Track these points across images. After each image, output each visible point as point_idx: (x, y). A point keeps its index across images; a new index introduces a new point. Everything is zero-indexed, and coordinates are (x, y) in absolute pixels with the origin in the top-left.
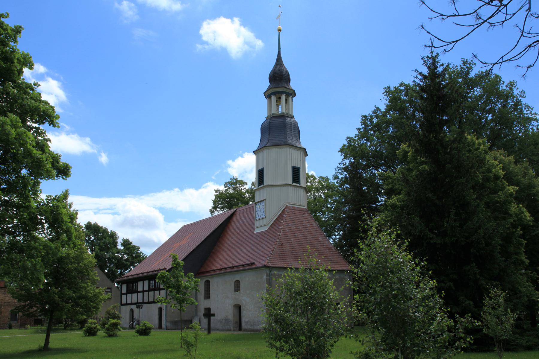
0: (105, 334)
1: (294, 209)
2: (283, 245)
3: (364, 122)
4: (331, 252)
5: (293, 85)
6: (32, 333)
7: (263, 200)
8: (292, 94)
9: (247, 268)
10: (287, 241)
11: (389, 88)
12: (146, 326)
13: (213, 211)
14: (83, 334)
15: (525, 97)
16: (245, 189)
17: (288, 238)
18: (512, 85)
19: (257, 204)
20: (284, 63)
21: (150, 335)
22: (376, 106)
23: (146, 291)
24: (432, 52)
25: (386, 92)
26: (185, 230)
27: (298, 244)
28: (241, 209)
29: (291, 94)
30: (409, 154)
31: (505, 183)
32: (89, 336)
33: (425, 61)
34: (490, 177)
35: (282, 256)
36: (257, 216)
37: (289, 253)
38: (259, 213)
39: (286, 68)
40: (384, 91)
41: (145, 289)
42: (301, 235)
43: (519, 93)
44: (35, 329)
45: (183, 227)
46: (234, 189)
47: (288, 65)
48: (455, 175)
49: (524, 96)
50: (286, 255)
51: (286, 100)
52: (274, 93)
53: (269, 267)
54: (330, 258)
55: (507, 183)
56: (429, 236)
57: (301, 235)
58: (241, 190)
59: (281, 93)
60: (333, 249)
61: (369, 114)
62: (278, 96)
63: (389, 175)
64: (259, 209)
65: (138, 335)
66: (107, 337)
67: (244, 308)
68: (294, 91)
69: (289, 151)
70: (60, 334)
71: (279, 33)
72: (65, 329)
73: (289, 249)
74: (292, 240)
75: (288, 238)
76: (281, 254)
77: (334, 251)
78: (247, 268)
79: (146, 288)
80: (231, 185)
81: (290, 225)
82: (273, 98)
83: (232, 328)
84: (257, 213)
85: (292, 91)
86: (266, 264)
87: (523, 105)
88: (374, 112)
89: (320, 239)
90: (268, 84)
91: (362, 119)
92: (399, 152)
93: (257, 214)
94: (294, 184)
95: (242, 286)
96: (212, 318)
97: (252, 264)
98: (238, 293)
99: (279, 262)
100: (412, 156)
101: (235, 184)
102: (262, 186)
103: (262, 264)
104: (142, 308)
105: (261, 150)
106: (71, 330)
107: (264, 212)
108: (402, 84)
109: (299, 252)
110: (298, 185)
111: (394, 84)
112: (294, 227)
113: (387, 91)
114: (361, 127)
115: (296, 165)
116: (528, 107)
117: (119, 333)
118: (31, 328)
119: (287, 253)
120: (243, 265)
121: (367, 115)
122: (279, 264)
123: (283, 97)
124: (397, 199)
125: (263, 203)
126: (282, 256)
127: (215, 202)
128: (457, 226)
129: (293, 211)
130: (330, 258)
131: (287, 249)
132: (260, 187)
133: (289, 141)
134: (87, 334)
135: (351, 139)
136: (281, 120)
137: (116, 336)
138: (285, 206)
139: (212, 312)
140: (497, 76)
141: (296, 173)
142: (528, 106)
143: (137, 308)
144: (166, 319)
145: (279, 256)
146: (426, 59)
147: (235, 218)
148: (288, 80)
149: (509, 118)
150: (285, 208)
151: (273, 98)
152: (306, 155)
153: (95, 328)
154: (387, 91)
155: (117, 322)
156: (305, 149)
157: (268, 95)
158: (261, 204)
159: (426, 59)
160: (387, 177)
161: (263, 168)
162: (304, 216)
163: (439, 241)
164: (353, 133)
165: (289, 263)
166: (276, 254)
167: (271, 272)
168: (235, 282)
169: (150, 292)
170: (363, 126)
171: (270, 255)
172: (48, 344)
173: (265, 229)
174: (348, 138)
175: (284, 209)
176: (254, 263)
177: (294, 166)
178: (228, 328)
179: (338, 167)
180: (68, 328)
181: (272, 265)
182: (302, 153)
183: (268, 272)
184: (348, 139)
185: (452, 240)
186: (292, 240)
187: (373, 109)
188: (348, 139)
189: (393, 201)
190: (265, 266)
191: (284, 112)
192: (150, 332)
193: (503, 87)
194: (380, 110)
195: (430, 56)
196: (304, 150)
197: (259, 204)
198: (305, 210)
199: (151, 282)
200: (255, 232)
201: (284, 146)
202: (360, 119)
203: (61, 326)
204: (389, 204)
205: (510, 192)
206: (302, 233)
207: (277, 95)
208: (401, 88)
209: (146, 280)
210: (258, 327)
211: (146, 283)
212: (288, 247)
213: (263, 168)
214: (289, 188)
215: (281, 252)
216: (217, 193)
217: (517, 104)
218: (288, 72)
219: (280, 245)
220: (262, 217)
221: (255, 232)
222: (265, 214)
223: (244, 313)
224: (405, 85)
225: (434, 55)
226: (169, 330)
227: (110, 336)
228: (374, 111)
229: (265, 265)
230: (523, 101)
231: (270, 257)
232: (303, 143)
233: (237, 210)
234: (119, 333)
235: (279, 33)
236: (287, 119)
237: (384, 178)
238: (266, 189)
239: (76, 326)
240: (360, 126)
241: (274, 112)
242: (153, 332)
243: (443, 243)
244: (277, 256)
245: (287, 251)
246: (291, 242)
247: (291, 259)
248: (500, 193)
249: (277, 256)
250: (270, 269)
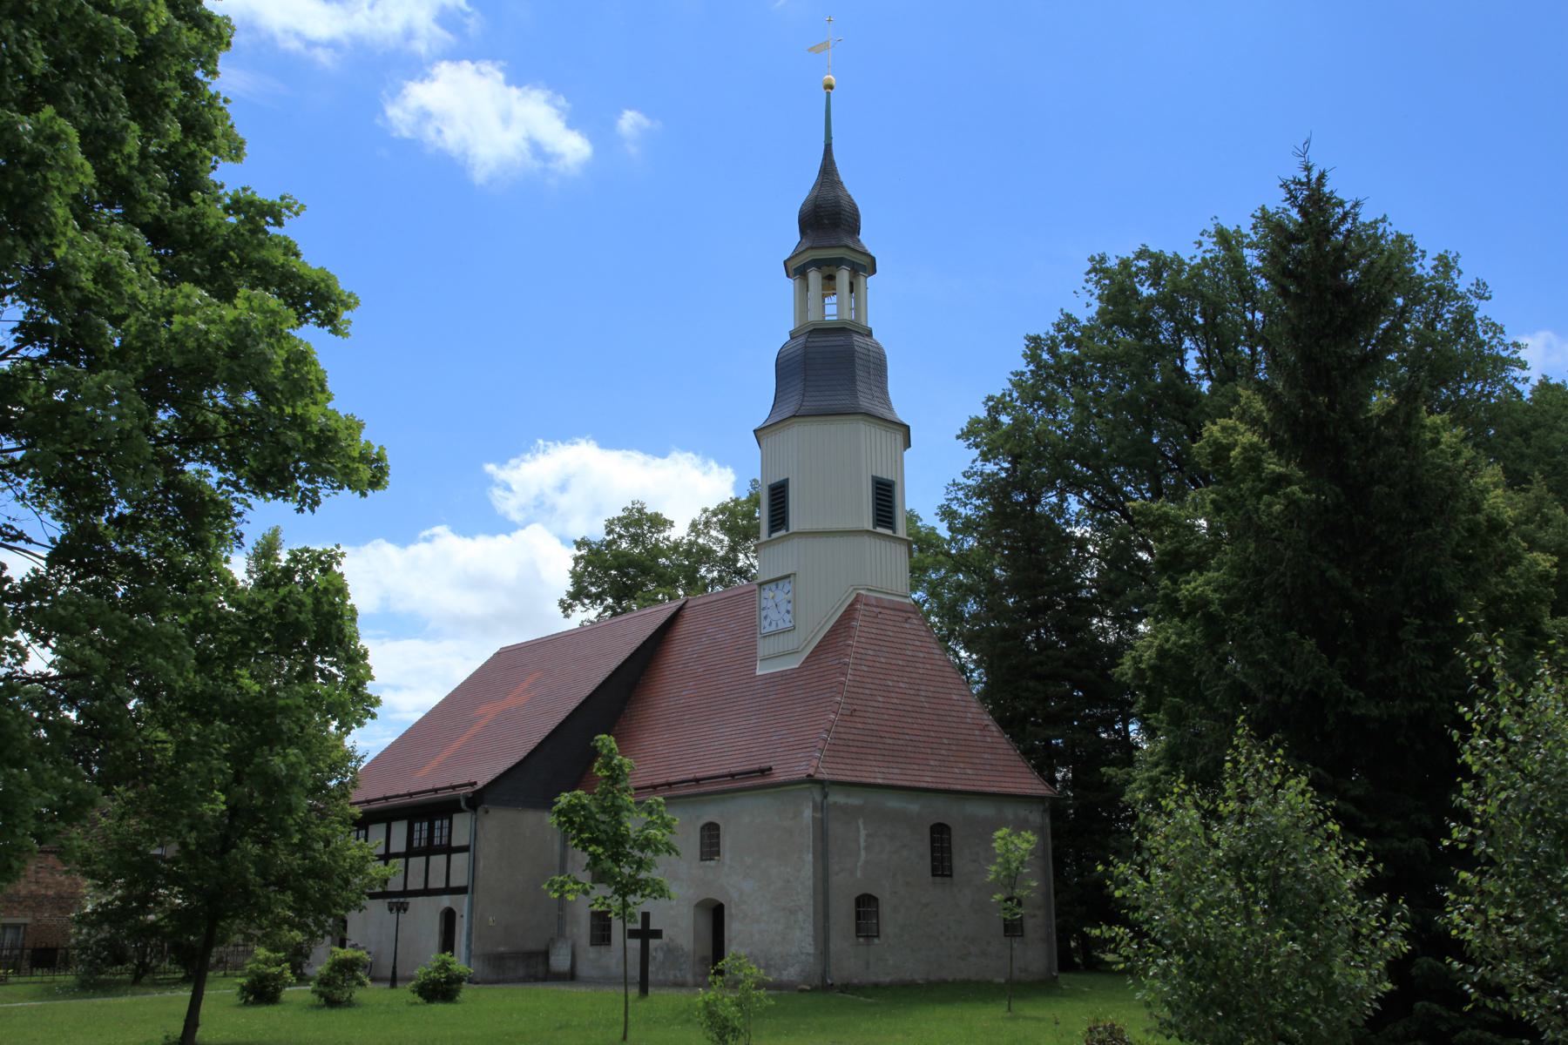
0: (315, 997)
1: (879, 604)
2: (857, 713)
3: (1033, 357)
4: (989, 739)
5: (869, 238)
6: (33, 998)
7: (788, 576)
8: (865, 266)
9: (748, 783)
10: (864, 703)
11: (1103, 259)
12: (447, 970)
13: (570, 606)
14: (238, 998)
15: (1490, 297)
16: (668, 539)
17: (867, 692)
18: (1445, 265)
19: (766, 587)
20: (843, 178)
21: (456, 1002)
22: (1065, 311)
23: (397, 855)
24: (1308, 169)
25: (1094, 270)
26: (507, 665)
27: (898, 713)
28: (701, 601)
29: (864, 268)
30: (1233, 453)
31: (1518, 544)
32: (253, 1004)
33: (1290, 192)
34: (1480, 523)
35: (854, 750)
36: (765, 623)
37: (874, 739)
38: (773, 614)
39: (849, 192)
40: (1088, 266)
41: (393, 850)
42: (901, 685)
43: (1473, 288)
44: (42, 982)
45: (498, 654)
46: (635, 540)
47: (855, 184)
48: (1404, 516)
49: (1487, 295)
50: (864, 744)
51: (851, 284)
52: (818, 264)
53: (821, 782)
54: (986, 756)
55: (1525, 544)
56: (1345, 694)
57: (901, 685)
58: (656, 545)
59: (838, 262)
60: (994, 729)
61: (1047, 333)
62: (827, 270)
63: (1165, 512)
64: (771, 603)
65: (419, 1000)
66: (319, 1007)
67: (733, 911)
68: (873, 260)
69: (866, 433)
70: (124, 1000)
71: (828, 94)
72: (137, 980)
73: (874, 727)
74: (880, 699)
75: (867, 692)
76: (851, 743)
77: (996, 734)
78: (748, 783)
79: (398, 844)
80: (626, 526)
81: (871, 652)
82: (814, 277)
83: (690, 978)
84: (764, 613)
85: (868, 260)
86: (811, 771)
87: (1479, 323)
88: (1059, 328)
89: (955, 697)
90: (794, 236)
91: (1027, 346)
92: (1200, 447)
93: (766, 618)
94: (879, 530)
95: (726, 842)
96: (653, 943)
97: (764, 772)
98: (712, 863)
99: (849, 767)
100: (1244, 459)
101: (638, 523)
102: (783, 533)
103: (800, 771)
104: (405, 910)
105: (781, 425)
106: (157, 985)
107: (788, 612)
108: (1143, 253)
109: (901, 736)
110: (889, 532)
111: (1119, 249)
112: (883, 660)
113: (1098, 267)
114: (1025, 370)
115: (885, 474)
116: (1497, 329)
117: (358, 994)
118: (21, 979)
119: (869, 739)
120: (732, 775)
121: (1043, 336)
122: (848, 773)
123: (843, 276)
124: (1208, 583)
125: (786, 586)
126: (854, 750)
127: (577, 577)
128: (1427, 667)
129: (879, 610)
130: (986, 756)
131: (868, 727)
132: (775, 535)
133: (865, 403)
134: (251, 998)
135: (997, 403)
136: (839, 340)
137: (349, 1004)
138: (854, 596)
139: (653, 926)
140: (1401, 239)
141: (885, 496)
142: (1494, 324)
143: (391, 910)
144: (468, 947)
145: (846, 749)
146: (1292, 187)
147: (683, 629)
148: (854, 227)
149: (1451, 354)
150: (856, 600)
151: (814, 277)
152: (907, 444)
153: (276, 977)
154: (1098, 267)
155: (357, 959)
156: (907, 428)
157: (797, 269)
158: (780, 586)
159: (1292, 187)
160: (1160, 517)
161: (787, 480)
162: (907, 626)
163: (1375, 712)
164: (1000, 385)
165: (877, 769)
166: (837, 742)
167: (825, 796)
168: (703, 828)
169: (412, 861)
170: (1031, 367)
171: (821, 744)
172: (195, 1031)
173: (794, 663)
174: (990, 398)
175: (851, 605)
176: (770, 769)
177: (879, 475)
178: (675, 976)
179: (954, 484)
180: (146, 979)
181: (830, 777)
182: (900, 438)
183: (818, 799)
184: (991, 403)
185: (1416, 706)
186: (880, 699)
187: (1056, 317)
188: (991, 403)
189: (1195, 589)
190: (810, 780)
191: (846, 316)
192: (457, 991)
193: (1424, 268)
194: (1076, 321)
195: (1304, 180)
196: (906, 429)
197: (773, 586)
198: (909, 609)
199: (417, 826)
200: (759, 673)
201: (851, 417)
202: (1021, 346)
203: (122, 973)
204: (1185, 597)
205: (1540, 568)
206: (906, 680)
207: (825, 268)
208: (1141, 263)
209: (398, 818)
210: (785, 973)
211: (400, 830)
212: (870, 721)
213: (787, 480)
214: (867, 540)
215: (852, 737)
216: (583, 552)
217: (1465, 319)
218: (854, 204)
219: (848, 712)
220: (782, 626)
221: (759, 673)
222: (794, 617)
223: (732, 928)
224: (1151, 255)
225: (1315, 175)
226: (477, 983)
227: (332, 1003)
228: (1058, 325)
229: (809, 775)
230: (1483, 310)
231: (822, 750)
232: (901, 410)
233: (689, 605)
234: (358, 994)
235: (828, 94)
236: (856, 338)
237: (1151, 519)
238: (795, 544)
239: (165, 973)
240: (1022, 365)
241: (813, 317)
242: (466, 992)
243: (1385, 717)
244: (841, 748)
245: (866, 732)
246: (876, 704)
247: (880, 758)
248: (1510, 571)
249: (841, 748)
250: (823, 788)
